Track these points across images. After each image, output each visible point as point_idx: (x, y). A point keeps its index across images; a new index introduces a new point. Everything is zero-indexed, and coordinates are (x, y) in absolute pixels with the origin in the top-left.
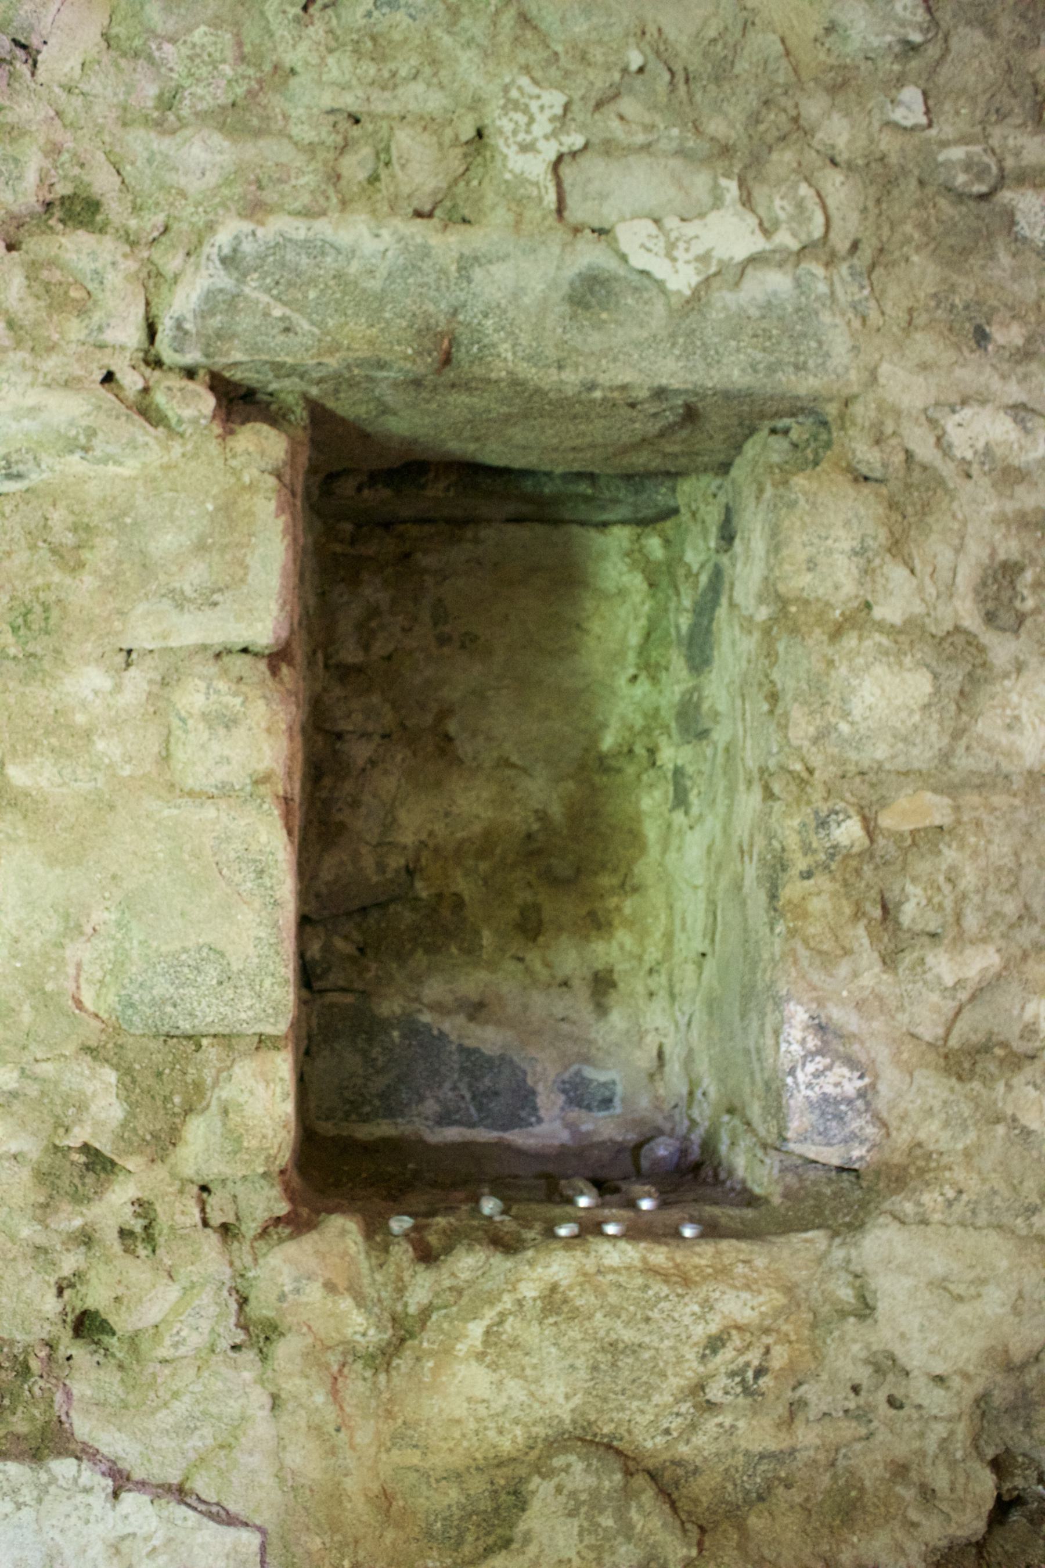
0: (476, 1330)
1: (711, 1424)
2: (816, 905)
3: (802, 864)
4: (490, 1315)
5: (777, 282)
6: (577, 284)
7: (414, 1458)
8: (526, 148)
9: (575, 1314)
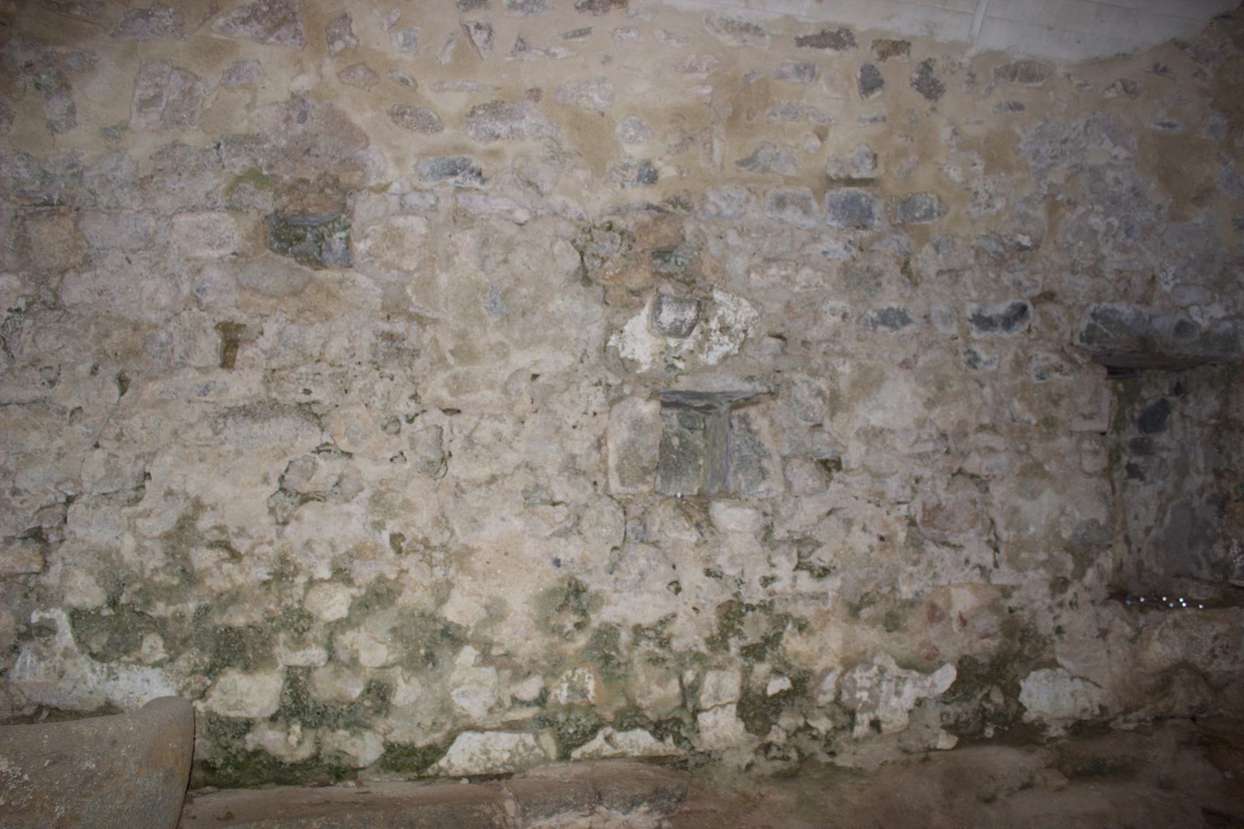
0: (1156, 632)
1: (1216, 662)
2: (1238, 510)
3: (1235, 498)
4: (1160, 627)
5: (1229, 325)
6: (921, 390)
7: (1142, 670)
8: (1167, 283)
9: (1182, 628)
